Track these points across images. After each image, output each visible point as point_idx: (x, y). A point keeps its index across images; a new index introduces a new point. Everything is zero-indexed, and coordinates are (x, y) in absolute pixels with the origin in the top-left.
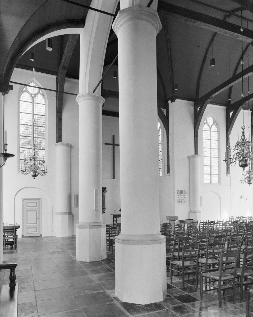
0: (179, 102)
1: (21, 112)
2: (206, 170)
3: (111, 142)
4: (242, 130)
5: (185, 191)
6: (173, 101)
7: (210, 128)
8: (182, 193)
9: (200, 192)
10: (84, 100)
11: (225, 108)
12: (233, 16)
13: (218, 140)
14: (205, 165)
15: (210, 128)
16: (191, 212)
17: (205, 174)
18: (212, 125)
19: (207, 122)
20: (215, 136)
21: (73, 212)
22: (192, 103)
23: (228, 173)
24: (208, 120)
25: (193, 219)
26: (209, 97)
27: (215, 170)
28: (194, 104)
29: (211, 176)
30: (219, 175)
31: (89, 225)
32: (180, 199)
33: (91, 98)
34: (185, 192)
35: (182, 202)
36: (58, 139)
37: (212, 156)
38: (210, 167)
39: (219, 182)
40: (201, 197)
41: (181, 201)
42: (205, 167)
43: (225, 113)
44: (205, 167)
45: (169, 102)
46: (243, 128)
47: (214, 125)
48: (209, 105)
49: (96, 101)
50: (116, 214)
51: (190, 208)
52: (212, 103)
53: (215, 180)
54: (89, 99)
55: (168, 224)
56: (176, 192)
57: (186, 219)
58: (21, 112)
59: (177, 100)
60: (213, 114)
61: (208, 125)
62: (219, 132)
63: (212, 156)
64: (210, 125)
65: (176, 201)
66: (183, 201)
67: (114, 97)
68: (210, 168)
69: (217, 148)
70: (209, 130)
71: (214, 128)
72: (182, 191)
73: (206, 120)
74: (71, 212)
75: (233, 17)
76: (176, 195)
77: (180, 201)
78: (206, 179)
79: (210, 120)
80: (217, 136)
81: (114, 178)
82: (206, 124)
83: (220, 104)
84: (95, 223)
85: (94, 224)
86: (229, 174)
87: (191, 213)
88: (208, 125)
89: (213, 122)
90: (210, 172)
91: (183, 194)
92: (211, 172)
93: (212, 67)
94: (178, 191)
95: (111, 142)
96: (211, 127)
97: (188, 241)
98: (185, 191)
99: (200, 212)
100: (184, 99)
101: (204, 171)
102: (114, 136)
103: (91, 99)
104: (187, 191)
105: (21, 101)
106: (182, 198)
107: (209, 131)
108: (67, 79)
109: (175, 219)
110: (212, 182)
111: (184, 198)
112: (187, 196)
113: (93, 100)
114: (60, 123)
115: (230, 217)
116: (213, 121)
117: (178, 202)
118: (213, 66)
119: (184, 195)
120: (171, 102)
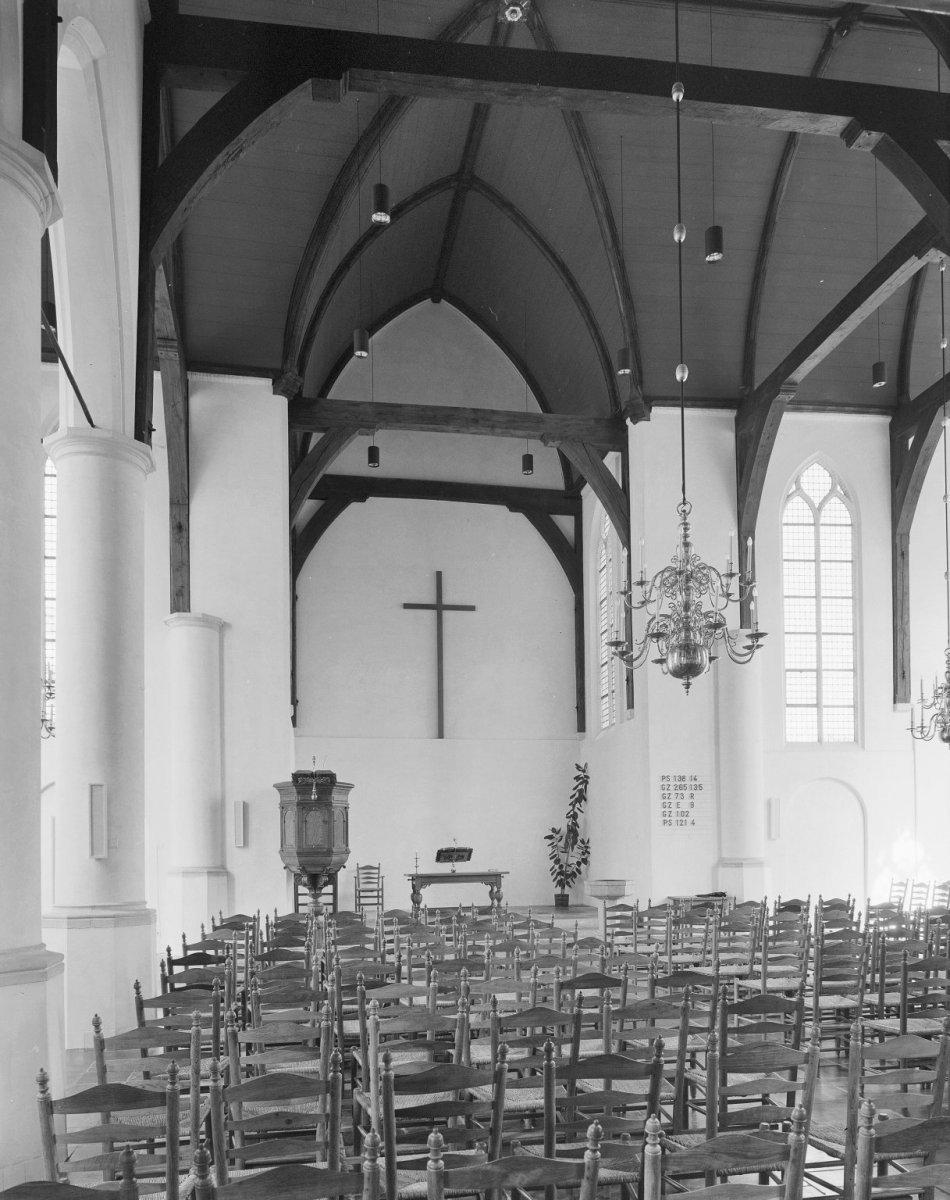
0: (664, 417)
1: (47, 516)
2: (799, 688)
3: (431, 599)
4: (679, 520)
5: (695, 779)
6: (640, 415)
7: (817, 511)
8: (683, 785)
9: (760, 780)
10: (85, 453)
11: (887, 420)
12: (861, 24)
13: (852, 561)
14: (793, 667)
15: (817, 511)
16: (722, 862)
17: (788, 705)
18: (826, 499)
19: (799, 488)
20: (838, 542)
21: (229, 867)
22: (730, 415)
23: (900, 694)
24: (804, 480)
25: (723, 894)
26: (781, 382)
27: (839, 688)
28: (738, 420)
29: (820, 714)
30: (858, 707)
31: (66, 916)
32: (674, 809)
33: (85, 448)
34: (693, 783)
35: (682, 823)
36: (175, 603)
37: (823, 631)
38: (814, 674)
39: (859, 739)
40: (769, 804)
41: (679, 819)
42: (791, 678)
43: (886, 441)
44: (791, 678)
45: (628, 421)
46: (684, 511)
47: (835, 500)
48: (789, 419)
49: (106, 455)
50: (424, 870)
51: (720, 849)
52: (798, 406)
53: (840, 725)
54: (77, 453)
55: (894, 907)
56: (655, 782)
57: (700, 893)
58: (47, 516)
59: (655, 410)
60: (825, 458)
61: (807, 500)
62: (856, 526)
63: (823, 631)
64: (817, 503)
65: (656, 818)
66: (689, 820)
67: (401, 428)
68: (815, 681)
69: (850, 594)
70: (812, 522)
71: (837, 511)
72: (682, 778)
73: (797, 482)
74: (223, 867)
75: (864, 28)
76: (656, 793)
77: (674, 819)
78: (799, 727)
79: (816, 480)
80: (850, 544)
81: (441, 735)
82: (797, 499)
83: (859, 406)
84: (93, 907)
85: (88, 912)
86: (906, 700)
87: (722, 870)
88: (807, 500)
89: (829, 487)
90: (815, 695)
91: (687, 793)
92: (819, 697)
93: (713, 262)
94: (663, 778)
95: (431, 599)
96: (820, 509)
97: (936, 975)
98: (695, 779)
99: (760, 864)
100: (699, 403)
101: (788, 695)
102: (439, 575)
103: (81, 453)
104: (706, 777)
105: (46, 475)
106: (685, 805)
107: (846, 525)
108: (195, 377)
109: (615, 893)
110: (825, 739)
111: (692, 805)
112: (705, 800)
113: (91, 453)
114: (180, 543)
115: (893, 884)
116: (829, 480)
117: (665, 822)
118: (716, 257)
119: (692, 796)
120: (635, 423)
